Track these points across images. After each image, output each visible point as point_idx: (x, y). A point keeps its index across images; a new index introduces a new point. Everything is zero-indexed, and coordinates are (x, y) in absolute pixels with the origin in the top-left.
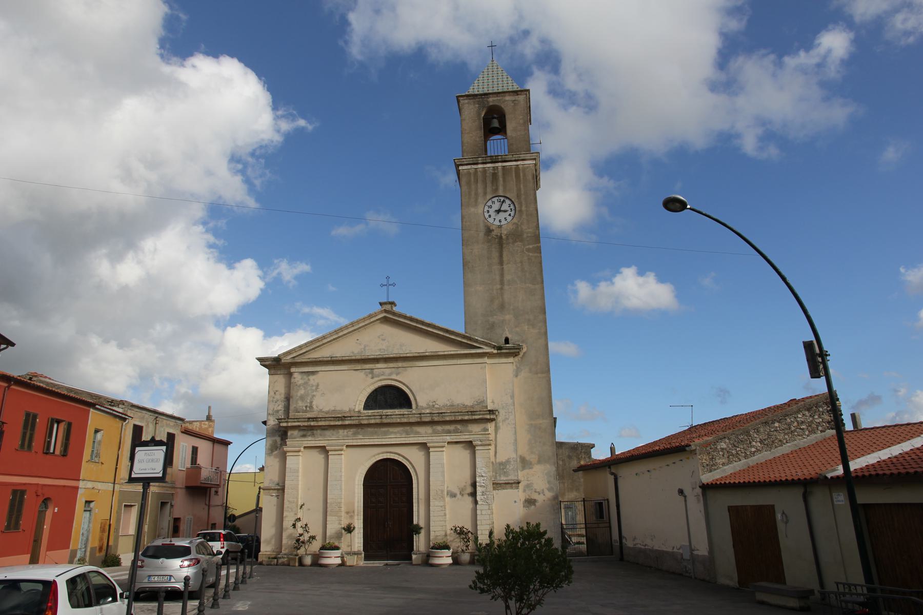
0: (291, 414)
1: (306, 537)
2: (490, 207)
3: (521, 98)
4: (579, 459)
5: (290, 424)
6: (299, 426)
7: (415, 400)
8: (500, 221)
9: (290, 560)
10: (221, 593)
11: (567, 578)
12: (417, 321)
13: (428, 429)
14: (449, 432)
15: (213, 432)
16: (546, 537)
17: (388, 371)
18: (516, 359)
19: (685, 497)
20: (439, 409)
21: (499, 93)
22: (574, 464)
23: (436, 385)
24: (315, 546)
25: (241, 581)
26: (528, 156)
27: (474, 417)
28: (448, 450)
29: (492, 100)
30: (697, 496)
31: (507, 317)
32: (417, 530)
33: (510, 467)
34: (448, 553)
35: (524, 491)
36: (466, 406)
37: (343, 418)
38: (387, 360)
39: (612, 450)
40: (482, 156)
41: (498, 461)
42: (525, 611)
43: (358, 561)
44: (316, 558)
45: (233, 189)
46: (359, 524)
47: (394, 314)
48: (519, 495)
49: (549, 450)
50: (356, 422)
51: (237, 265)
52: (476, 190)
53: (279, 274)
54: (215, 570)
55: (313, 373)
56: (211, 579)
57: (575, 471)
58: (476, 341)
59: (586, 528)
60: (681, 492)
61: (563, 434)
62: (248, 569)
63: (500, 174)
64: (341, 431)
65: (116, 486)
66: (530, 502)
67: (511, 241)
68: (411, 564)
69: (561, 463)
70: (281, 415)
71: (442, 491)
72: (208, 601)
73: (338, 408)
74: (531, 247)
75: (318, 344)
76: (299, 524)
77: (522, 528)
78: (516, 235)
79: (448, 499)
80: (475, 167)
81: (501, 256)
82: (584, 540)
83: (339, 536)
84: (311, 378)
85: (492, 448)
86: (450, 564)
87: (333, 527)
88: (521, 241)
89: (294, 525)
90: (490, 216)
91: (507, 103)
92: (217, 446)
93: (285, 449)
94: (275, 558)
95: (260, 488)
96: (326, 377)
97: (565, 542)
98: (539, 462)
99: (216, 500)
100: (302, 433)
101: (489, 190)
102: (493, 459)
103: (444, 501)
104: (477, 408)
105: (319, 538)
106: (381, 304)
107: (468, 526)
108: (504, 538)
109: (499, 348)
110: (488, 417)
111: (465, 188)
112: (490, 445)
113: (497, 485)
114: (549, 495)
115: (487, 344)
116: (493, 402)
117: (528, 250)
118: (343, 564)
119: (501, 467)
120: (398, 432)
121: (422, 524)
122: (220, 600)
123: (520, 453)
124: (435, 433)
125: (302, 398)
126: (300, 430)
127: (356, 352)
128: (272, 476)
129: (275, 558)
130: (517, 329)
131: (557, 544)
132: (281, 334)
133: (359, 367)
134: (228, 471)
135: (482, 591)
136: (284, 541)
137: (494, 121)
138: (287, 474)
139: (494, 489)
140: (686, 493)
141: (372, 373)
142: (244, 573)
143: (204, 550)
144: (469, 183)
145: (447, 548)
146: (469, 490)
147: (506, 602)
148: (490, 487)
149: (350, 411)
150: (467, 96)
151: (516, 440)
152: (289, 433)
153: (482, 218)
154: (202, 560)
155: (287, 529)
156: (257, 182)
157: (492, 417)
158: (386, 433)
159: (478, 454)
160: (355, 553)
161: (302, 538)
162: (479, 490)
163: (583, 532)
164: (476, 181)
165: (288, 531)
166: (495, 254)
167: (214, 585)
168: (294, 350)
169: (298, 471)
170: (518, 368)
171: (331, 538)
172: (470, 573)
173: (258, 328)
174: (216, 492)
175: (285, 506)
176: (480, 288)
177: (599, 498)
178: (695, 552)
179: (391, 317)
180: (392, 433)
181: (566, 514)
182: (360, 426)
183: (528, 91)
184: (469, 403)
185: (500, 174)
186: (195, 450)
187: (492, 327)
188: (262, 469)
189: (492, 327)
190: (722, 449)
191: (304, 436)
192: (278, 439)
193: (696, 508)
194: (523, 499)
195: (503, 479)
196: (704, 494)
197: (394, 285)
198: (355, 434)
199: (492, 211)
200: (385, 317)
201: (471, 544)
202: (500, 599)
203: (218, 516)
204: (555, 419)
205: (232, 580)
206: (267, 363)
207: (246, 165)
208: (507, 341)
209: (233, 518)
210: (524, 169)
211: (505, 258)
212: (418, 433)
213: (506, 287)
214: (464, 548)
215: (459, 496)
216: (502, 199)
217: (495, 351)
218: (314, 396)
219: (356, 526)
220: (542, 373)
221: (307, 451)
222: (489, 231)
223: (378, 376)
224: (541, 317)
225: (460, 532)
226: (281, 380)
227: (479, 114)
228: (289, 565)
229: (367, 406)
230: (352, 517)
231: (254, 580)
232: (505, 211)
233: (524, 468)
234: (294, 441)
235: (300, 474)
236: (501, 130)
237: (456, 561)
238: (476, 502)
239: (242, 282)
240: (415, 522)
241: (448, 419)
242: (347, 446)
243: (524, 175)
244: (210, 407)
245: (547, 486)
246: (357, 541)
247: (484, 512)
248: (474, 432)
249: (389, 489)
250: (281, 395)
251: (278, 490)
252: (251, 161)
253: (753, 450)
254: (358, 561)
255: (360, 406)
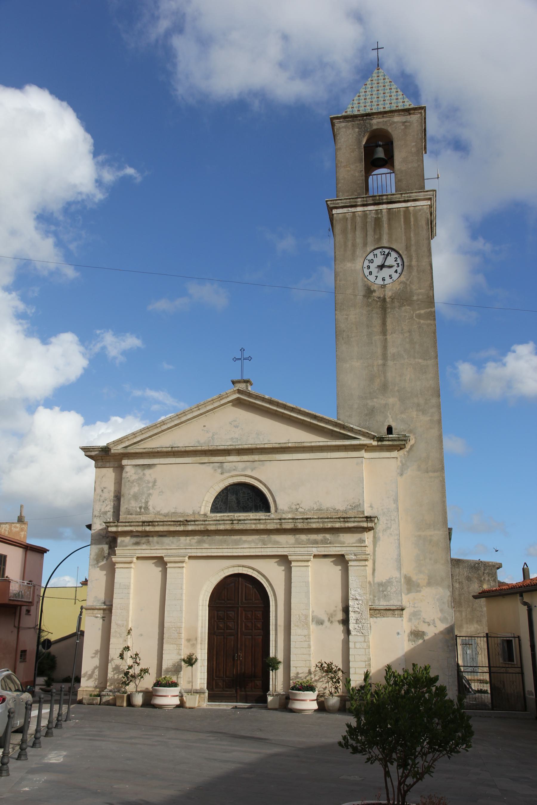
0: (122, 517)
1: (136, 670)
2: (372, 261)
3: (415, 118)
4: (481, 582)
5: (120, 529)
6: (132, 532)
7: (275, 501)
8: (383, 279)
9: (115, 699)
10: (30, 739)
11: (465, 740)
12: (278, 404)
13: (290, 539)
14: (316, 542)
15: (25, 537)
16: (438, 684)
17: (241, 465)
18: (401, 452)
20: (303, 513)
21: (386, 112)
22: (475, 588)
23: (300, 484)
24: (148, 682)
25: (56, 723)
26: (421, 195)
27: (347, 525)
28: (314, 564)
29: (376, 123)
31: (391, 400)
32: (274, 664)
33: (391, 589)
34: (312, 695)
35: (410, 620)
36: (337, 511)
37: (186, 522)
38: (240, 452)
39: (525, 572)
40: (365, 195)
41: (377, 580)
42: (410, 781)
43: (200, 702)
44: (149, 697)
45: (44, 251)
46: (202, 655)
47: (250, 395)
48: (404, 625)
49: (442, 569)
50: (201, 528)
51: (53, 340)
52: (354, 239)
53: (104, 348)
54: (24, 710)
55: (149, 466)
56: (19, 722)
57: (475, 597)
58: (351, 430)
59: (490, 673)
61: (460, 548)
62: (65, 708)
63: (385, 219)
64: (182, 539)
66: (416, 634)
67: (396, 304)
68: (266, 708)
69: (457, 585)
70: (110, 517)
71: (306, 616)
72: (13, 751)
73: (180, 510)
74: (422, 312)
75: (156, 431)
76: (128, 655)
77: (406, 671)
78: (404, 298)
79: (313, 627)
81: (384, 324)
82: (487, 687)
83: (177, 669)
84: (148, 472)
85: (369, 563)
86: (315, 710)
87: (170, 659)
88: (409, 305)
89: (121, 656)
90: (371, 273)
91: (395, 126)
92: (30, 554)
93: (114, 559)
94: (99, 695)
95: (82, 608)
96: (165, 471)
97: (463, 688)
98: (429, 584)
99: (27, 621)
100: (135, 540)
101: (370, 239)
102: (370, 578)
103: (309, 628)
104: (351, 514)
105: (153, 671)
106: (234, 383)
107: (338, 663)
108: (384, 682)
109: (381, 439)
110: (365, 525)
111: (339, 237)
112: (366, 560)
113: (375, 612)
114: (442, 627)
115: (365, 435)
116: (371, 506)
117: (419, 316)
118: (182, 705)
119: (382, 588)
120: (253, 541)
121: (280, 657)
122: (29, 749)
123: (404, 571)
124: (299, 543)
125: (136, 497)
126: (132, 536)
127: (202, 442)
128: (96, 594)
129: (99, 695)
130: (403, 416)
131: (452, 694)
132: (106, 420)
133: (205, 459)
134: (43, 585)
135: (355, 750)
136: (110, 675)
137: (378, 151)
138: (115, 591)
139: (372, 616)
141: (222, 467)
142: (59, 715)
143: (11, 686)
144: (344, 231)
145: (311, 688)
146: (340, 616)
147: (386, 766)
148: (367, 613)
149: (194, 513)
150: (345, 117)
151: (399, 555)
152: (120, 540)
153: (361, 275)
154: (8, 698)
155: (112, 659)
156: (72, 246)
157: (370, 525)
158: (237, 543)
159: (351, 570)
160: (197, 692)
161: (131, 672)
162: (352, 616)
163: (487, 677)
164: (354, 229)
165: (115, 660)
166: (377, 322)
167: (21, 730)
168: (126, 438)
169: (128, 587)
170: (403, 465)
171: (167, 671)
172: (339, 725)
173: (78, 412)
174: (28, 611)
175: (112, 630)
176: (357, 364)
177: (507, 634)
179: (246, 402)
180: (245, 542)
181: (464, 653)
182: (206, 533)
183: (424, 108)
184: (341, 507)
185: (385, 219)
187: (371, 412)
188: (85, 583)
189: (371, 412)
191: (137, 544)
192: (106, 547)
194: (408, 631)
195: (382, 604)
197: (249, 359)
198: (199, 542)
199: (373, 266)
200: (238, 399)
201: (341, 685)
202: (377, 762)
203: (29, 642)
204: (450, 530)
205: (44, 723)
206: (93, 454)
207: (57, 223)
208: (390, 430)
209: (48, 643)
210: (416, 213)
211: (389, 327)
212: (277, 543)
213: (390, 363)
214: (333, 690)
215: (327, 623)
216: (387, 251)
217: (375, 443)
218: (150, 495)
219: (199, 658)
220: (434, 471)
221: (140, 562)
222: (369, 291)
223: (229, 471)
224: (434, 401)
225: (328, 670)
226: (109, 473)
227: (359, 142)
228: (115, 705)
229: (215, 508)
230: (194, 646)
231: (71, 723)
232: (390, 267)
233: (409, 591)
234: (125, 548)
235: (132, 591)
236: (388, 162)
237: (322, 707)
238: (348, 632)
239: (62, 358)
240: (272, 655)
241: (314, 526)
242: (190, 557)
243: (416, 220)
245: (440, 615)
246: (200, 675)
247: (358, 645)
248: (346, 543)
249: (241, 615)
250: (110, 494)
251: (104, 610)
252: (63, 219)
254: (200, 702)
255: (206, 508)
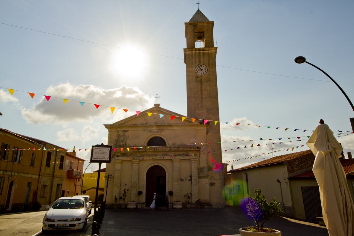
8: (201, 74)
19: (280, 183)
30: (286, 182)
41: (200, 167)
60: (278, 181)
65: (40, 176)
80: (192, 52)
84: (126, 133)
125: (122, 141)
140: (281, 181)
174: (79, 180)
178: (285, 205)
186: (71, 163)
190: (296, 164)
193: (286, 187)
194: (143, 192)
196: (290, 182)
197: (159, 97)
223: (153, 133)
244: (74, 147)
253: (308, 165)
